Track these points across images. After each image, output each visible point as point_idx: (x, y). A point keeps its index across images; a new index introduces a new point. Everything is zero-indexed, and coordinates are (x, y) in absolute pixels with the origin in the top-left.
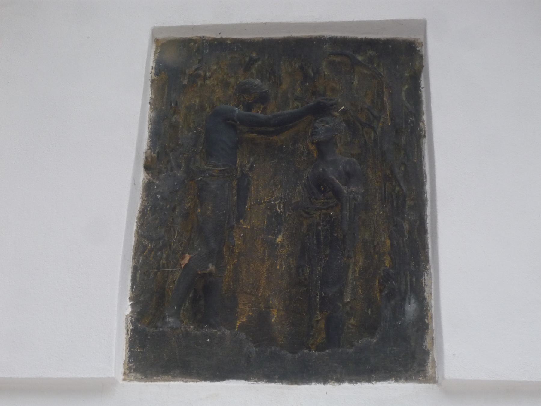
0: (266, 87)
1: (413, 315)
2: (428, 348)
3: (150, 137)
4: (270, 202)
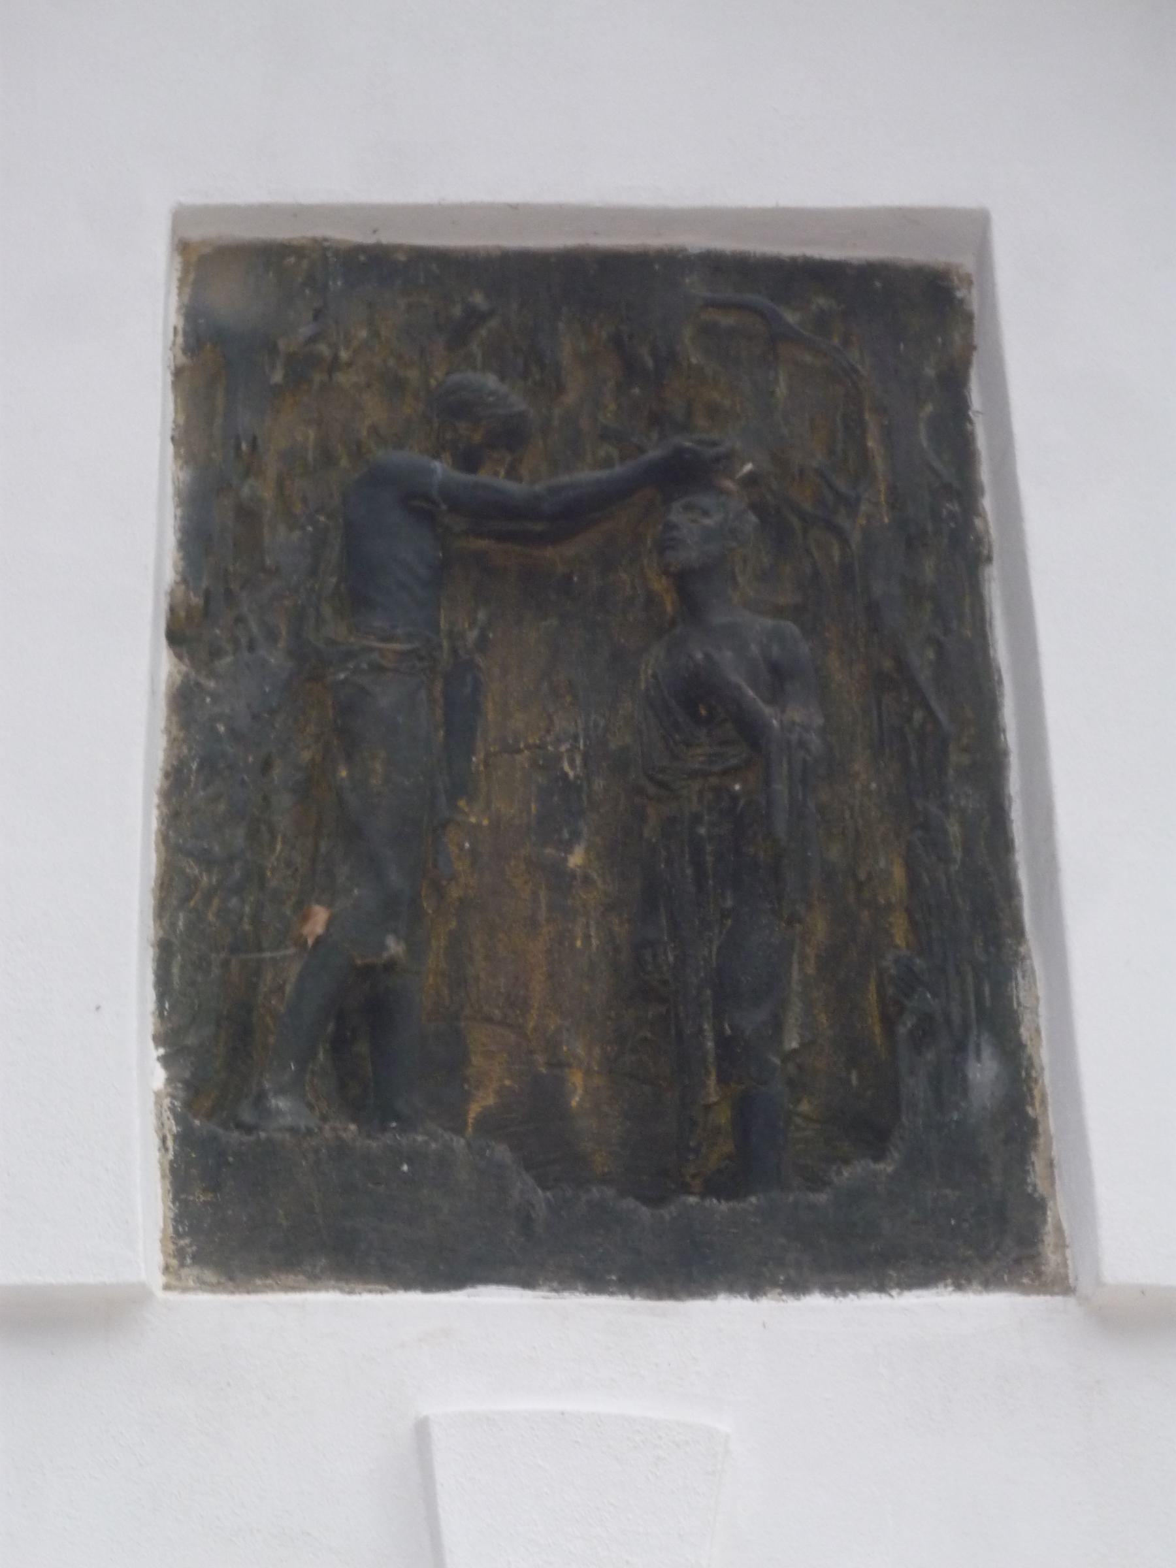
0: (518, 402)
3: (182, 545)
4: (542, 746)
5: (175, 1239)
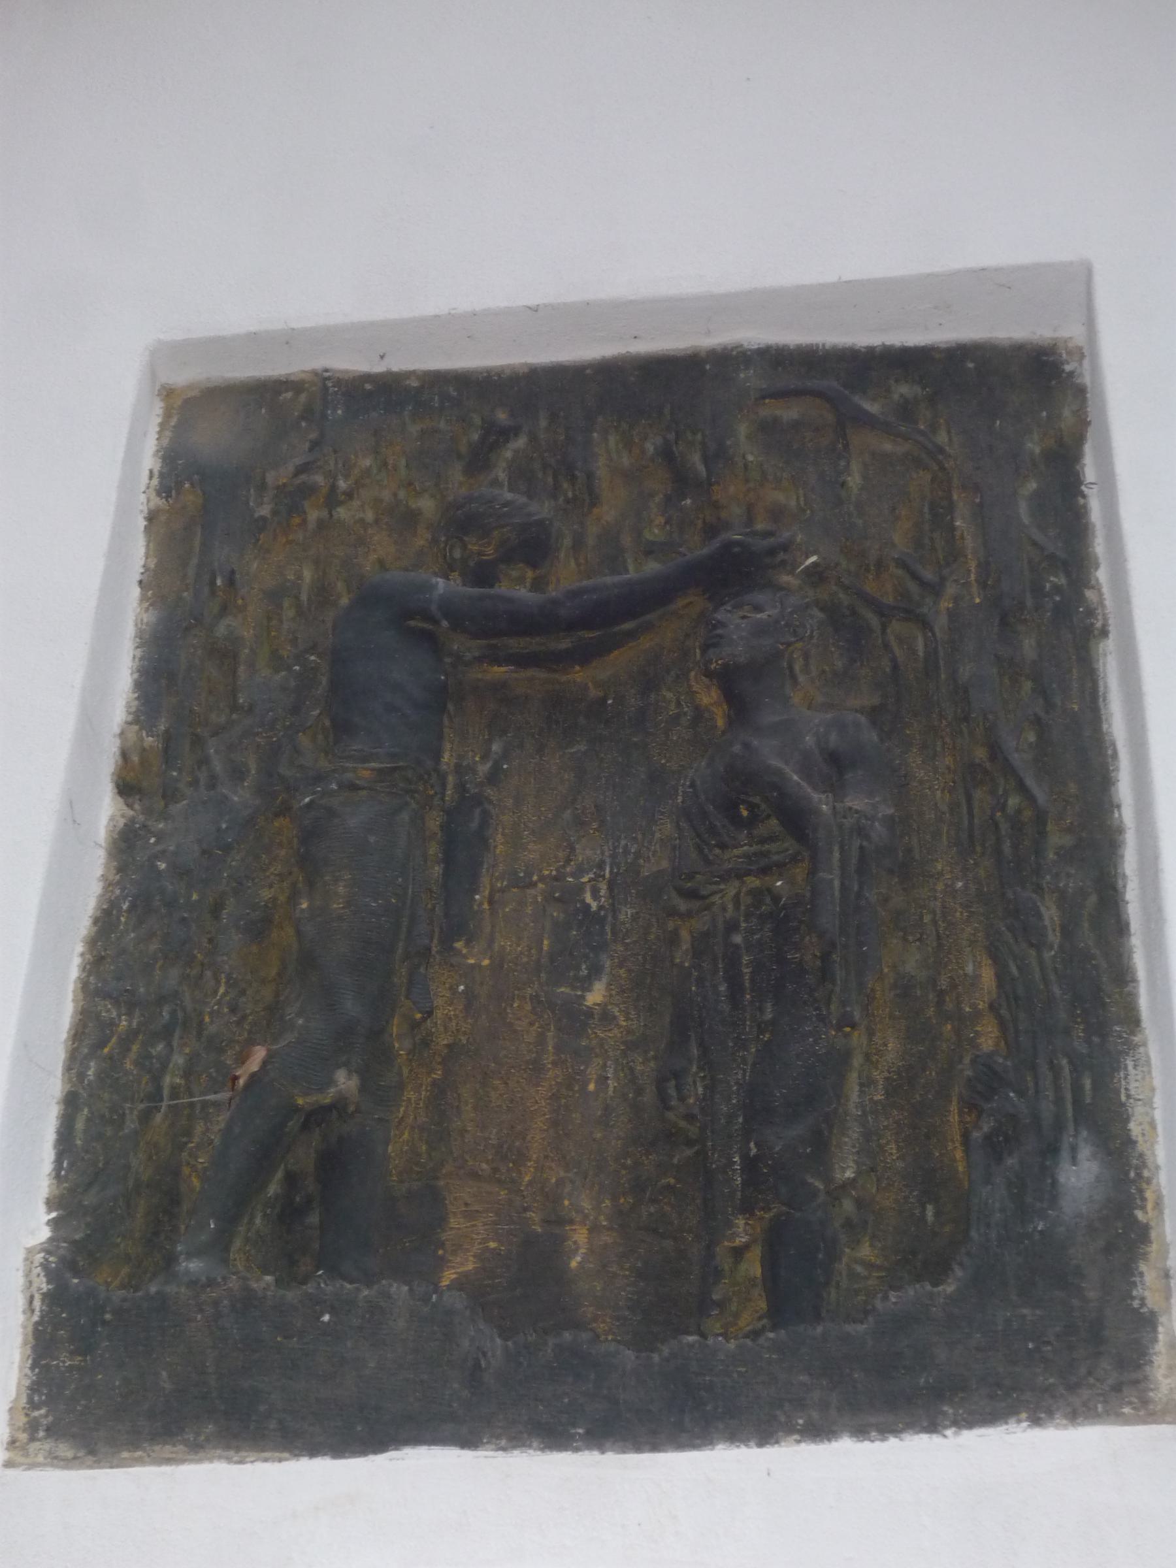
1: (1090, 1197)
2: (1150, 1306)
5: (28, 1409)
